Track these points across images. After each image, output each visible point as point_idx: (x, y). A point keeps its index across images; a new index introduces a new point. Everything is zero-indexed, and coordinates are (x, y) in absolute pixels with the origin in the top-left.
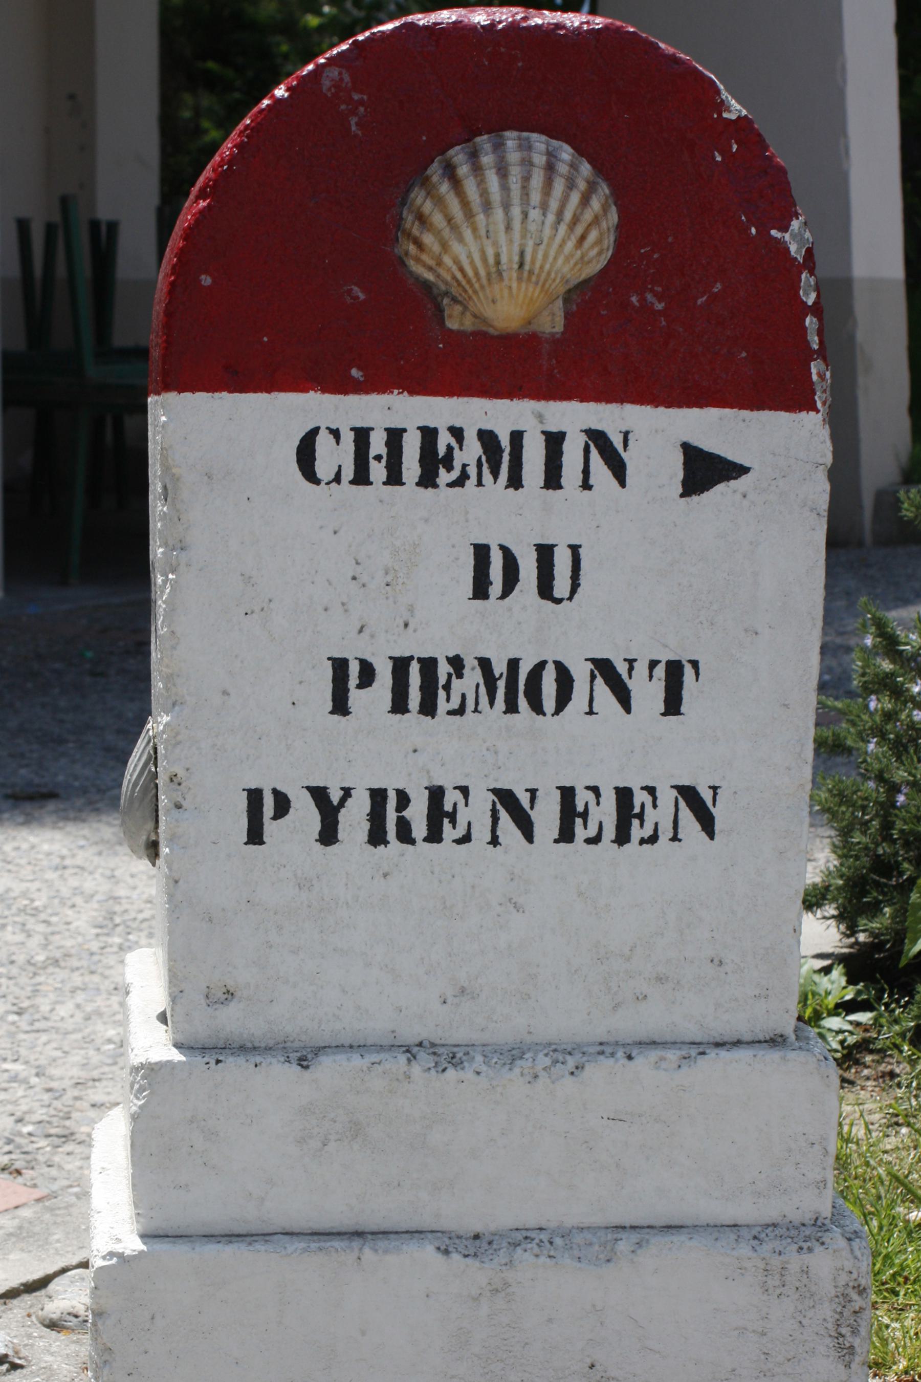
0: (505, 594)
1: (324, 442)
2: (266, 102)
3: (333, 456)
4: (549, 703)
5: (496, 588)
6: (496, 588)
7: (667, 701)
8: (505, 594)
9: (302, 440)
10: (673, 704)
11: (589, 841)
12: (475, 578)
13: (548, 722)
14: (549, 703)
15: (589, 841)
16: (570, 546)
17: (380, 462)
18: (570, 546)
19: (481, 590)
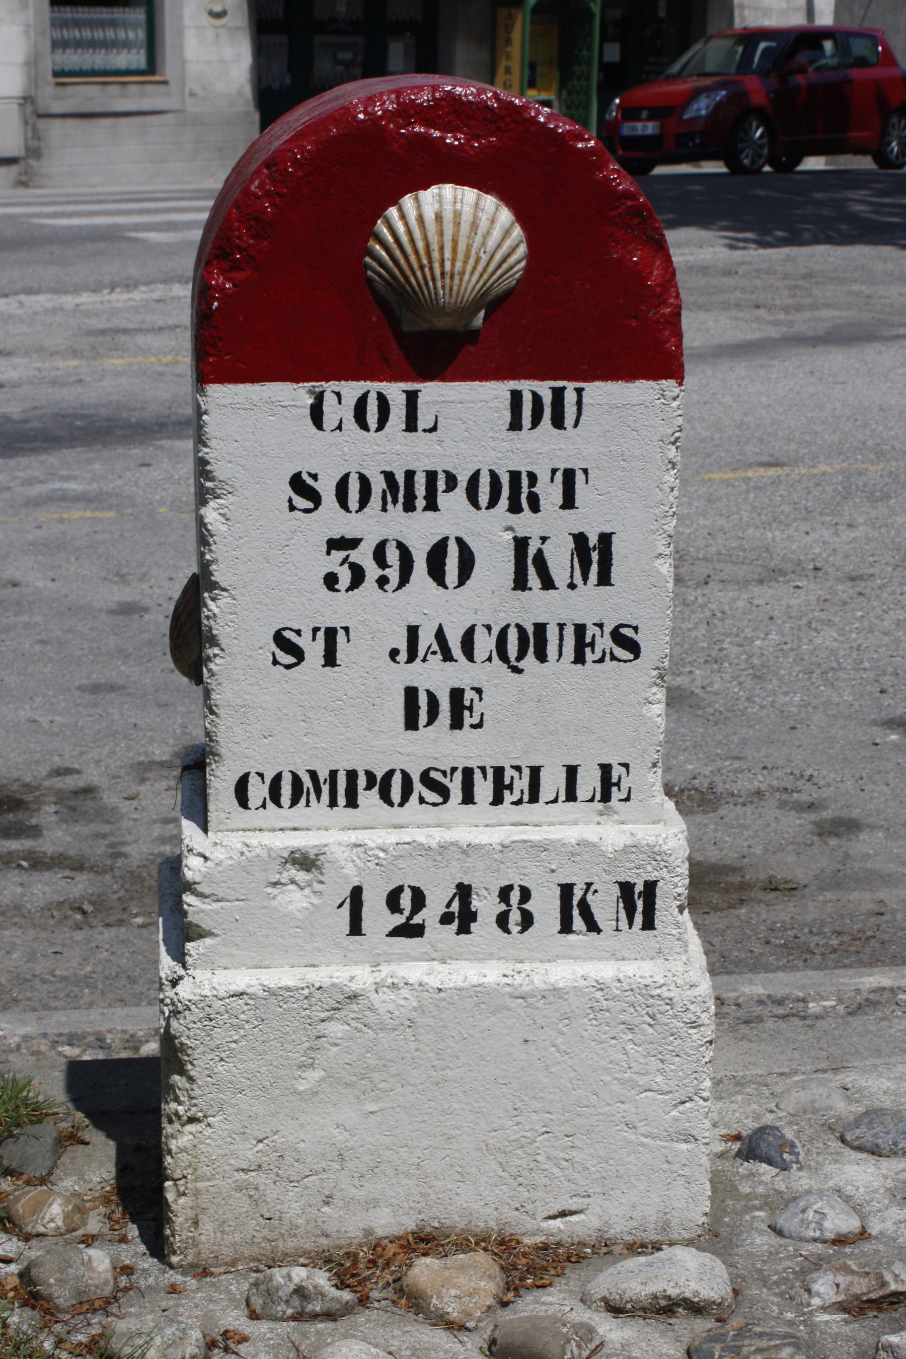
0: (346, 477)
1: (253, 780)
2: (437, 134)
3: (551, 493)
4: (453, 551)
5: (423, 717)
6: (423, 717)
7: (515, 581)
8: (346, 477)
9: (468, 577)
10: (330, 659)
11: (473, 726)
12: (409, 638)
13: (353, 469)
14: (453, 551)
15: (473, 726)
16: (559, 624)
17: (583, 389)
18: (559, 624)
19: (515, 425)
